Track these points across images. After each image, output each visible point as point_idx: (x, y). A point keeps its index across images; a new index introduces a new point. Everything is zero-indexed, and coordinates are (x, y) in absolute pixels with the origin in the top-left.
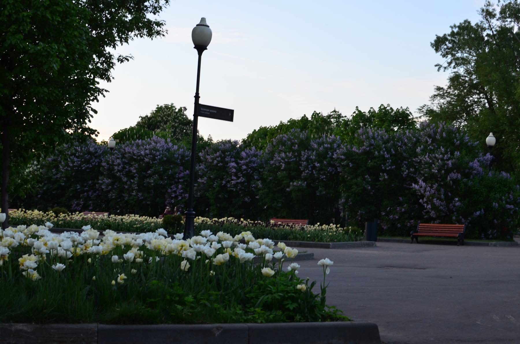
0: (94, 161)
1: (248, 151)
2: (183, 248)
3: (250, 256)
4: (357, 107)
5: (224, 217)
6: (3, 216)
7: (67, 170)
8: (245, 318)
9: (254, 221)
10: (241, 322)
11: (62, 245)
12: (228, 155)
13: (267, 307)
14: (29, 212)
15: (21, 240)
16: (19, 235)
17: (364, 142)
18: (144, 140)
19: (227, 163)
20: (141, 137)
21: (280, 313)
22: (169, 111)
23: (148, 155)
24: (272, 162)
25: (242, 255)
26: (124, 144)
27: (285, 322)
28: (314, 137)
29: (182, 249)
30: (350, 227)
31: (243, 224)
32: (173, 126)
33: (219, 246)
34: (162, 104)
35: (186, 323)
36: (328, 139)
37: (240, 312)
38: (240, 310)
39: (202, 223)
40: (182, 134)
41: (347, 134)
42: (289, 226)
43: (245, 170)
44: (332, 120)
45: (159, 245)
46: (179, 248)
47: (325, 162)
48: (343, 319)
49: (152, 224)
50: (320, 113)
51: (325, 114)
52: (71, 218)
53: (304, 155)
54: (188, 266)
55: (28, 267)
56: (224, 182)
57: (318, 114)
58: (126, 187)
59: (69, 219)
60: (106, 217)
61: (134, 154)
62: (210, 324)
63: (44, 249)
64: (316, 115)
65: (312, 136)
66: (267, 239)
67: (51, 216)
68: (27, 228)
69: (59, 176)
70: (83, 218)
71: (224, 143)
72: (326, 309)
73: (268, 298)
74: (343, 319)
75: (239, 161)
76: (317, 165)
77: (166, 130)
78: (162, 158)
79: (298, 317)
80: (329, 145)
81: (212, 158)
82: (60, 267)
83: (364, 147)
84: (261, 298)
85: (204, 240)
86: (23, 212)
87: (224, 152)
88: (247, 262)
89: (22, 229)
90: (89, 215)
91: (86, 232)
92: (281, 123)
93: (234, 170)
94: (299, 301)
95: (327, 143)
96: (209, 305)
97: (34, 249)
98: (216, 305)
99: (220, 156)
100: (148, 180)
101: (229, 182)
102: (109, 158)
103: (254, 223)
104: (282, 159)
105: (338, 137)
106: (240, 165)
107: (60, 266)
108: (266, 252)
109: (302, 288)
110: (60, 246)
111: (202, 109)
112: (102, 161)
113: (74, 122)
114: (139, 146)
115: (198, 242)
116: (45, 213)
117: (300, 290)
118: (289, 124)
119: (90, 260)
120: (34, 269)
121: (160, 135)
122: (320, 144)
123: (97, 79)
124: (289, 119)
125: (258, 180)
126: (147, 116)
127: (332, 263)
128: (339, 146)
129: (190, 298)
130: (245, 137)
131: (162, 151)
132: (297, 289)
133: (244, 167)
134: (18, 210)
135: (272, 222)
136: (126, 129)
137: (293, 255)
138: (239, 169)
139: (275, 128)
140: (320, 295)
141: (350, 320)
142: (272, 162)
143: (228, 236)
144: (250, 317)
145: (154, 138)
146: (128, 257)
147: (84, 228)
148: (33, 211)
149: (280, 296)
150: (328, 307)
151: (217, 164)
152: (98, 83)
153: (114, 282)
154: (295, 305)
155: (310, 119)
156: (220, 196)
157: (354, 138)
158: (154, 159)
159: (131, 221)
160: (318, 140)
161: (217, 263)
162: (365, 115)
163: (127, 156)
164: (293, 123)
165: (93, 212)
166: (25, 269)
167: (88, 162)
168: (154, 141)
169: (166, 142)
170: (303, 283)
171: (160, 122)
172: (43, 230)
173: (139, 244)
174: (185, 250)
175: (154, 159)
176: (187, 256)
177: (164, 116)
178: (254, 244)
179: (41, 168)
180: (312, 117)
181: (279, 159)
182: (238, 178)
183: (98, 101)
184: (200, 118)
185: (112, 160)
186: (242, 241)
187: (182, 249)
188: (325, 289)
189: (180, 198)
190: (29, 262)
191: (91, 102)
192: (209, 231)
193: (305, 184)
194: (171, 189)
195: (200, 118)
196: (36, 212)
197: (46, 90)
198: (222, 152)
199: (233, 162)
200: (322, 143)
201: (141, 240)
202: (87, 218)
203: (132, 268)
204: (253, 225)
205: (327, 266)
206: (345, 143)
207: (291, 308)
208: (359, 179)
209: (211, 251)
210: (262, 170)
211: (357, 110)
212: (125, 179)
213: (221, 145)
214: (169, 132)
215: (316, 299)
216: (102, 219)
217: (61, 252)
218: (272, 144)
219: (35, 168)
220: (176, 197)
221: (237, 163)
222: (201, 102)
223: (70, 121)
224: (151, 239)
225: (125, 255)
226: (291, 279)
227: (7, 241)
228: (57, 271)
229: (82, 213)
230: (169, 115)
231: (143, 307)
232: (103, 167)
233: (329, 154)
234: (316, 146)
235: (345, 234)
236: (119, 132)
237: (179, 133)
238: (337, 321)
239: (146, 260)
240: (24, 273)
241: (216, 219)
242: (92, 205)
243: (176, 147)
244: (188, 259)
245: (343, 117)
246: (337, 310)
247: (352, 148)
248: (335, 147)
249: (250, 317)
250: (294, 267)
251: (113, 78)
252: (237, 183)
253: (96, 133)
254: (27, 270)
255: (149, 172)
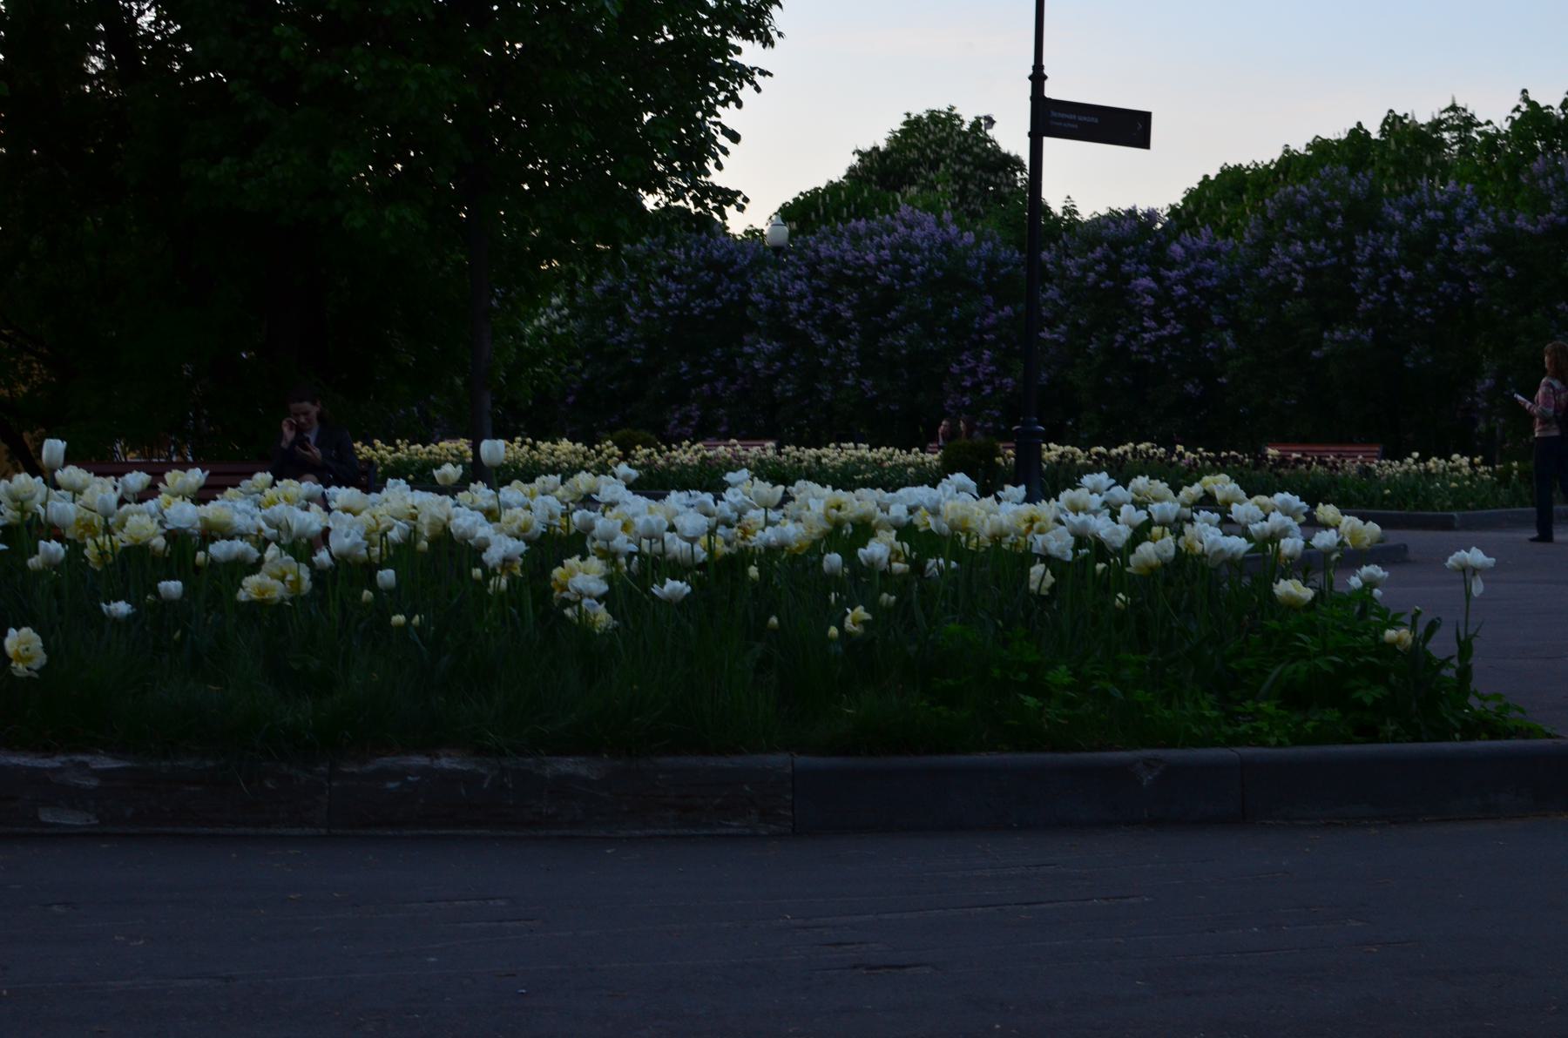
0: (728, 289)
1: (1189, 242)
2: (1036, 526)
3: (1238, 544)
4: (1524, 91)
5: (1124, 444)
6: (496, 448)
7: (647, 318)
8: (1229, 731)
9: (1218, 453)
10: (1215, 745)
11: (678, 526)
12: (1130, 256)
13: (1294, 698)
14: (545, 446)
15: (551, 516)
16: (545, 503)
17: (1550, 197)
18: (873, 218)
19: (1127, 279)
20: (862, 212)
21: (1333, 715)
22: (943, 130)
23: (886, 263)
24: (1264, 272)
25: (1214, 542)
26: (813, 233)
27: (1348, 742)
28: (1391, 189)
29: (1030, 528)
30: (1515, 464)
31: (1183, 464)
32: (958, 176)
33: (1142, 516)
34: (920, 110)
35: (1053, 749)
36: (1437, 194)
37: (1215, 713)
38: (1213, 708)
39: (1058, 463)
40: (985, 199)
41: (1496, 177)
42: (1324, 463)
43: (1183, 298)
44: (1446, 135)
45: (964, 519)
46: (1024, 527)
47: (1429, 266)
48: (1527, 733)
49: (910, 470)
50: (1406, 116)
51: (1423, 118)
52: (668, 459)
53: (1364, 246)
54: (1050, 579)
55: (581, 594)
56: (1119, 338)
57: (1401, 119)
58: (826, 362)
59: (661, 462)
60: (770, 453)
61: (845, 264)
62: (1125, 749)
63: (622, 542)
64: (1393, 123)
65: (1385, 189)
66: (1287, 495)
67: (610, 456)
68: (562, 483)
69: (624, 337)
70: (704, 458)
71: (1114, 218)
72: (1474, 701)
73: (1295, 672)
74: (1527, 733)
75: (1163, 272)
76: (1406, 275)
77: (935, 188)
78: (930, 270)
79: (1390, 727)
80: (1440, 214)
81: (1079, 267)
82: (675, 588)
83: (1553, 215)
84: (1275, 673)
85: (1096, 500)
86: (526, 448)
87: (1116, 245)
88: (1233, 563)
89: (549, 486)
90: (721, 448)
91: (737, 490)
92: (1287, 151)
93: (1149, 301)
94: (1393, 677)
95: (1434, 206)
96: (1117, 693)
97: (594, 539)
98: (1140, 695)
99: (1106, 258)
100: (890, 340)
101: (1133, 336)
102: (772, 277)
103: (1218, 458)
104: (1295, 261)
105: (1468, 187)
106: (1167, 283)
107: (674, 587)
108: (1285, 532)
109: (1399, 640)
110: (672, 528)
111: (1054, 114)
112: (749, 287)
113: (673, 172)
114: (860, 238)
115: (1081, 505)
116: (591, 447)
117: (1392, 645)
118: (1310, 153)
119: (753, 571)
120: (599, 599)
121: (920, 204)
122: (1412, 211)
123: (733, 40)
124: (1310, 140)
125: (1223, 327)
126: (876, 149)
127: (1491, 561)
128: (1471, 215)
129: (1061, 675)
130: (1177, 199)
131: (930, 251)
132: (1385, 644)
133: (1180, 290)
134: (512, 441)
135: (1272, 452)
136: (816, 189)
137: (1368, 541)
138: (1164, 296)
139: (1267, 167)
140: (1455, 662)
141: (1549, 736)
142: (1264, 272)
143: (1161, 487)
144: (1244, 728)
145: (903, 212)
146: (872, 556)
147: (730, 477)
148: (554, 442)
149: (1333, 663)
150: (1481, 697)
151: (1097, 283)
152: (738, 51)
153: (833, 631)
154: (1379, 691)
155: (1375, 135)
156: (1109, 380)
157: (1517, 191)
158: (904, 276)
159: (845, 463)
160: (1404, 198)
161: (1137, 568)
162: (1550, 116)
163: (823, 269)
164: (1321, 147)
165: (733, 441)
166: (572, 598)
167: (708, 291)
168: (902, 219)
169: (940, 223)
170: (1403, 625)
171: (917, 164)
172: (611, 488)
173: (898, 518)
174: (1041, 532)
175: (904, 276)
176: (1045, 549)
177: (928, 145)
178: (1245, 509)
179: (574, 316)
180: (1383, 130)
181: (1288, 260)
182: (1163, 323)
183: (739, 105)
184: (1048, 142)
185: (780, 283)
186: (1208, 501)
187: (1030, 528)
188: (1469, 640)
189: (988, 389)
190: (584, 576)
191: (719, 109)
192: (1104, 475)
193: (1367, 336)
194: (960, 363)
195: (1048, 142)
196: (565, 445)
197: (586, 78)
198: (1111, 245)
199: (1144, 275)
200: (1421, 207)
201: (904, 508)
202: (716, 457)
203: (881, 591)
204: (1214, 464)
205: (1475, 570)
206: (1487, 204)
207: (1368, 700)
208: (1537, 315)
209: (1118, 533)
210: (1235, 297)
211: (1526, 99)
212: (820, 340)
213: (1107, 227)
214: (945, 190)
215: (1444, 672)
216: (761, 461)
217: (676, 545)
218: (1264, 216)
219: (555, 316)
220: (977, 387)
221: (1158, 279)
222: (1052, 91)
223: (660, 168)
224: (938, 502)
225: (861, 551)
226: (1363, 613)
227: (515, 519)
228: (667, 603)
229: (700, 445)
230: (943, 143)
231: (924, 703)
232: (755, 304)
233: (1440, 241)
234: (1399, 217)
235: (1499, 484)
236: (796, 200)
237: (976, 196)
238: (1507, 738)
239: (917, 567)
240: (568, 612)
241: (1102, 449)
242: (725, 419)
243: (969, 237)
244: (1048, 559)
245: (1480, 124)
246: (1507, 706)
247: (1512, 218)
248: (1460, 217)
249: (1244, 728)
250: (1371, 575)
251: (780, 34)
252: (1161, 339)
253: (739, 200)
254: (579, 603)
255: (893, 314)
